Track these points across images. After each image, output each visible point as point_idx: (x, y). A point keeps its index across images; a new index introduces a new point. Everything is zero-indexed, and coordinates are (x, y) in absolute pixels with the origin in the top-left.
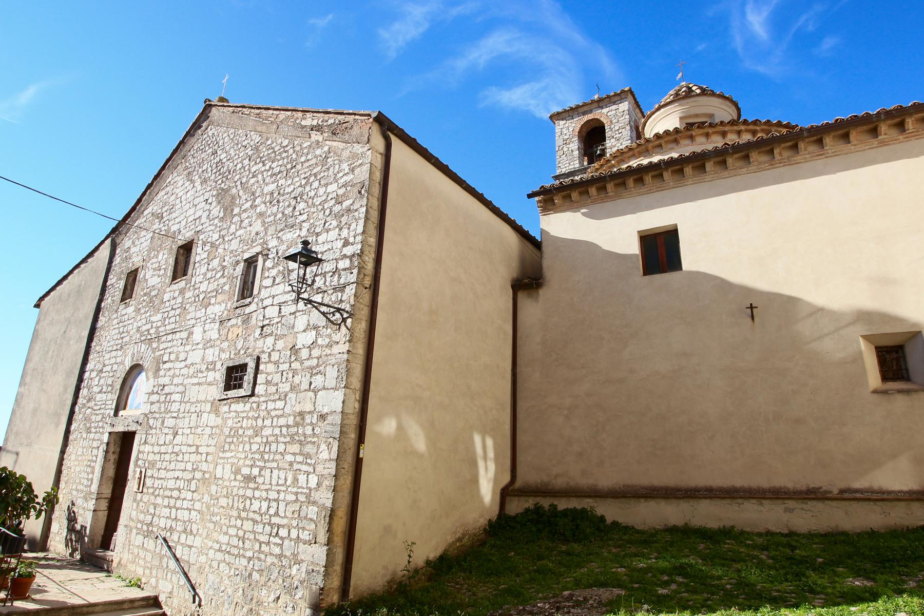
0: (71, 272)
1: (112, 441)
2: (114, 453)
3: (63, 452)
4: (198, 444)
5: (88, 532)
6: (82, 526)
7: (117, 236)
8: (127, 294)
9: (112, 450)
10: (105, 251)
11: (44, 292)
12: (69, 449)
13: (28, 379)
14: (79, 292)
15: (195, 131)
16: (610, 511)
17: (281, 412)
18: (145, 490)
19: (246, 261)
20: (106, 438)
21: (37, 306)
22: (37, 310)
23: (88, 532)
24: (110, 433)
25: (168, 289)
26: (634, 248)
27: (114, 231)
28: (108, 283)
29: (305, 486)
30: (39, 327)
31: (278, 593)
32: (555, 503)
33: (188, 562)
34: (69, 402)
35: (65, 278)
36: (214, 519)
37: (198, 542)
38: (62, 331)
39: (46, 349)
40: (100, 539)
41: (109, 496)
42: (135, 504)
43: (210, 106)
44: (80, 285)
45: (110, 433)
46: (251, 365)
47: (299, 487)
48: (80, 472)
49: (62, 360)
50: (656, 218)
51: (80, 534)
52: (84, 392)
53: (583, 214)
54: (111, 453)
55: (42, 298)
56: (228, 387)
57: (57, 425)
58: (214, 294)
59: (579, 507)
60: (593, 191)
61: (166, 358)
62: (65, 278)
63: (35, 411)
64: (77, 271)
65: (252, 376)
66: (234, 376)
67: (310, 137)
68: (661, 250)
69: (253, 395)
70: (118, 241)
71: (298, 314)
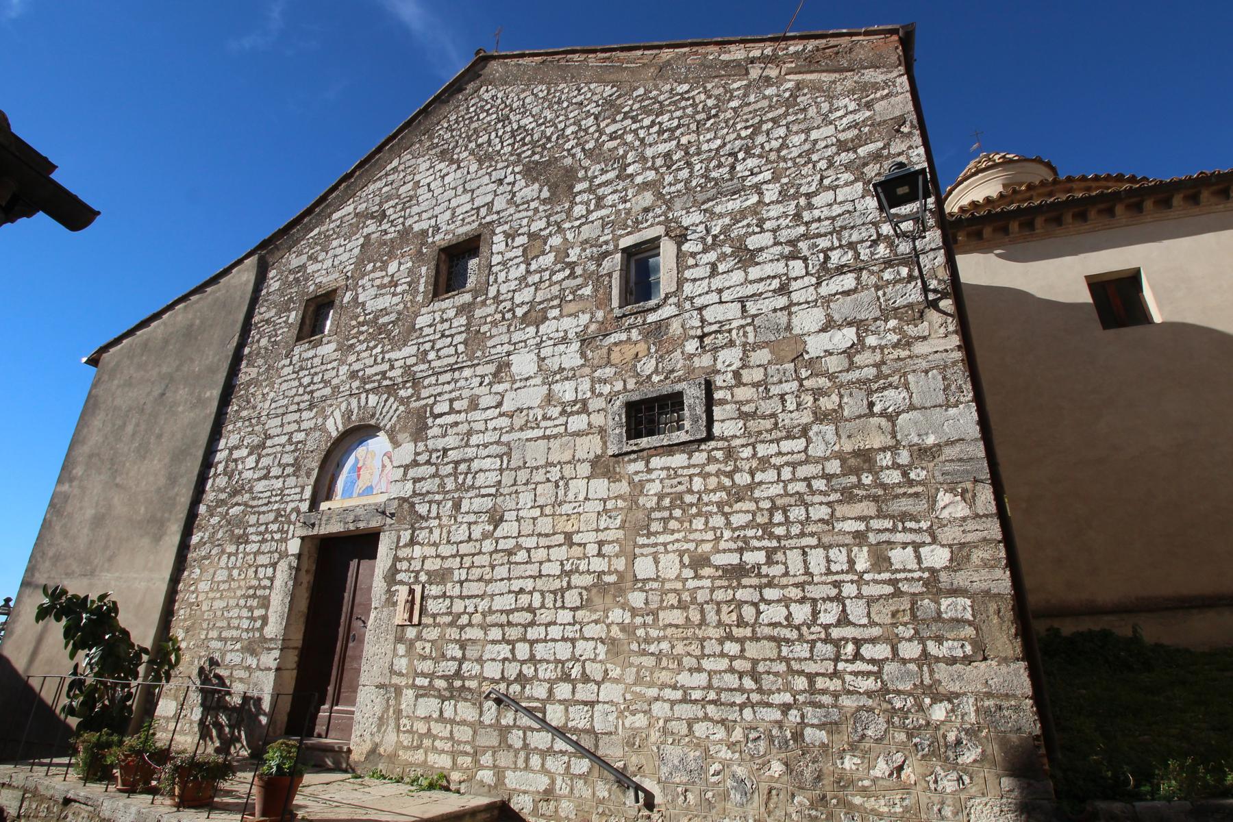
0: (170, 307)
1: (306, 553)
2: (307, 571)
3: (175, 579)
4: (569, 529)
5: (266, 706)
6: (246, 699)
7: (271, 252)
8: (310, 328)
9: (305, 567)
10: (245, 276)
11: (111, 338)
12: (192, 573)
13: (78, 471)
14: (189, 334)
15: (452, 95)
16: (1152, 631)
17: (803, 456)
18: (424, 620)
19: (624, 250)
20: (294, 546)
21: (94, 361)
22: (92, 370)
23: (266, 706)
24: (303, 538)
25: (424, 310)
26: (1085, 297)
27: (264, 245)
28: (256, 319)
29: (916, 567)
30: (99, 391)
31: (899, 758)
32: (1056, 626)
33: (591, 731)
34: (185, 500)
35: (157, 316)
36: (653, 648)
37: (610, 692)
38: (156, 393)
39: (119, 422)
40: (285, 719)
41: (299, 644)
42: (401, 649)
43: (487, 59)
44: (191, 325)
45: (303, 538)
46: (693, 395)
47: (897, 571)
48: (227, 608)
49: (160, 436)
50: (1110, 260)
51: (246, 712)
52: (217, 482)
53: (997, 255)
54: (303, 572)
55: (105, 349)
56: (634, 432)
57: (157, 539)
58: (556, 302)
59: (1097, 628)
60: (1014, 226)
61: (442, 407)
62: (157, 316)
63: (98, 521)
64: (181, 305)
65: (700, 410)
66: (647, 416)
67: (747, 73)
68: (1118, 298)
69: (710, 437)
70: (271, 260)
71: (794, 309)
